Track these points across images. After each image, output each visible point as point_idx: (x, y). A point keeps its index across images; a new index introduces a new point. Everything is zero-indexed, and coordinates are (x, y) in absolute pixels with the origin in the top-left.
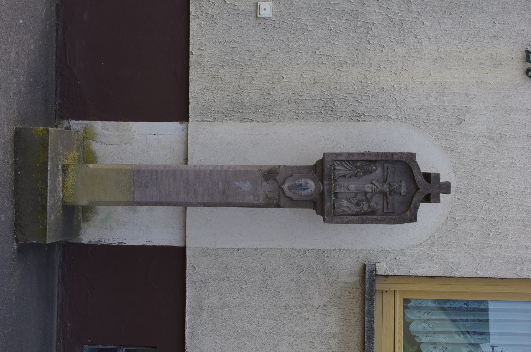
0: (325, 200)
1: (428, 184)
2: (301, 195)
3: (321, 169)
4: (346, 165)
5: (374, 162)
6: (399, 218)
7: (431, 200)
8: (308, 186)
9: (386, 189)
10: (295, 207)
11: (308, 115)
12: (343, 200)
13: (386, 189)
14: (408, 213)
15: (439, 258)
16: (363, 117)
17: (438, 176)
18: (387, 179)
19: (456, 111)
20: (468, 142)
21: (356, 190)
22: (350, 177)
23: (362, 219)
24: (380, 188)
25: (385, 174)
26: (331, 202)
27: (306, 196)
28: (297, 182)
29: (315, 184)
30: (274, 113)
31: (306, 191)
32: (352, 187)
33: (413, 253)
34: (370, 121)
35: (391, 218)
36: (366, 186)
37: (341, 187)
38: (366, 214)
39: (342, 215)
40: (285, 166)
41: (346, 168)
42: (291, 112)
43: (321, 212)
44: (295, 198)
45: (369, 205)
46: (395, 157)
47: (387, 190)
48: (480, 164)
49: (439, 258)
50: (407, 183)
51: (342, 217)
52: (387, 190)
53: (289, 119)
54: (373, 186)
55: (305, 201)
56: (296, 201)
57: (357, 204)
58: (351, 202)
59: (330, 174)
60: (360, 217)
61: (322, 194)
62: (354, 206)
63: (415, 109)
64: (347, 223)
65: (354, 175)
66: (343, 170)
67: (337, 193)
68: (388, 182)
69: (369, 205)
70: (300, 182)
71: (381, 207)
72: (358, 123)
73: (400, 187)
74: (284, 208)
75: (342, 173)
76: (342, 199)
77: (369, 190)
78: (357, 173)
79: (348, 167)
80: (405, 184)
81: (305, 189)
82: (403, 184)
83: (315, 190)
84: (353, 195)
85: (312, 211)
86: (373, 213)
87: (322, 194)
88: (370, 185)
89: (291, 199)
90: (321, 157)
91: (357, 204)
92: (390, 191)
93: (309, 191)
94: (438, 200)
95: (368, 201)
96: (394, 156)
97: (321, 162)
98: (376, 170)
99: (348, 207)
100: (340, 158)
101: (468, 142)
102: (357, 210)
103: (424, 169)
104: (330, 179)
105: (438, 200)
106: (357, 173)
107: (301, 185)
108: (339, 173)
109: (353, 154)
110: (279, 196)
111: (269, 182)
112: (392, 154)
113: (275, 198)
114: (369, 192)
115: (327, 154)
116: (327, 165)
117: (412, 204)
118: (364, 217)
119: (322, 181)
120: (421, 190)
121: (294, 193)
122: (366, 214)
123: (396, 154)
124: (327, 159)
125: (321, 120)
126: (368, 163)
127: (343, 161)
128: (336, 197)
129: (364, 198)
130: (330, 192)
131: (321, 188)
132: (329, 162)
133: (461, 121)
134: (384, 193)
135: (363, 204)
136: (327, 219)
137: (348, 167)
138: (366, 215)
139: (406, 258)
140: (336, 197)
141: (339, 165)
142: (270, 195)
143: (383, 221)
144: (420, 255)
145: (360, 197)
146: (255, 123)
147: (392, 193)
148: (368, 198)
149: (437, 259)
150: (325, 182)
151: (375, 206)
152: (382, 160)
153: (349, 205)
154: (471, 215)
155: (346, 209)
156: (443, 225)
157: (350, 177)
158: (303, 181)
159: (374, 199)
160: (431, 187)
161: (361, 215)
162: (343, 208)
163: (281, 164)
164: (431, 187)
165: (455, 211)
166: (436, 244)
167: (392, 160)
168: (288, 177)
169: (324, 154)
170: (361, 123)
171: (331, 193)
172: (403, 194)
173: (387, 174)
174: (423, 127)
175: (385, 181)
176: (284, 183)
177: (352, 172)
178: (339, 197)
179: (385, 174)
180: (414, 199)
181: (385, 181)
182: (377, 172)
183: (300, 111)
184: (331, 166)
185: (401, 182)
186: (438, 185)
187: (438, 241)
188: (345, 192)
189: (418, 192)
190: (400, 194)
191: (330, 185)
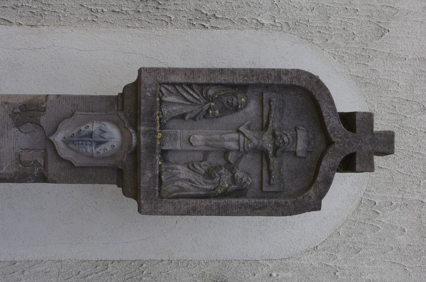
0: (142, 166)
1: (350, 134)
2: (92, 156)
3: (135, 102)
4: (185, 94)
5: (243, 88)
6: (294, 203)
7: (358, 167)
8: (106, 136)
9: (267, 143)
10: (79, 182)
11: (115, 15)
12: (179, 167)
13: (267, 143)
14: (311, 192)
15: (347, 272)
16: (213, 20)
17: (369, 117)
18: (268, 123)
19: (375, 14)
20: (395, 69)
21: (206, 145)
22: (194, 119)
23: (217, 204)
24: (255, 141)
25: (265, 113)
26: (153, 169)
27: (103, 158)
28: (83, 128)
29: (122, 133)
30: (50, 9)
31: (102, 147)
32: (199, 139)
33: (302, 264)
34: (226, 28)
35: (276, 203)
36: (226, 137)
37: (176, 139)
38: (226, 194)
39: (177, 197)
40: (58, 96)
41: (189, 101)
42: (83, 10)
43: (133, 191)
44: (78, 161)
45: (233, 177)
46: (284, 78)
47: (269, 146)
48: (415, 107)
49: (347, 272)
50: (308, 131)
51: (176, 201)
52: (269, 146)
53: (79, 21)
54: (242, 137)
55: (101, 168)
56: (82, 168)
57: (209, 175)
58: (195, 171)
59: (152, 113)
60: (214, 201)
61: (135, 153)
62: (201, 179)
63: (304, 9)
64: (188, 213)
65: (203, 113)
66: (179, 104)
67: (166, 151)
68: (270, 130)
69: (233, 177)
70: (90, 129)
71: (256, 180)
72: (204, 31)
73: (295, 139)
74: (55, 182)
75: (176, 109)
76: (177, 163)
77: (233, 145)
78: (207, 111)
79: (189, 97)
80: (304, 133)
81: (99, 143)
82: (301, 134)
83: (121, 146)
84: (199, 156)
85: (113, 190)
86: (240, 192)
87: (135, 153)
88: (235, 136)
89: (70, 163)
90: (133, 78)
91: (209, 175)
92: (276, 148)
93: (108, 147)
94: (369, 167)
95: (231, 168)
96: (283, 77)
97: (134, 89)
98: (246, 105)
99: (190, 181)
100: (173, 79)
101: (395, 69)
102: (209, 187)
103: (343, 105)
104: (153, 122)
105: (369, 167)
106: (207, 111)
107: (91, 135)
108: (170, 109)
109: (199, 70)
110: (45, 158)
111: (23, 128)
112: (279, 73)
113: (36, 161)
114: (232, 151)
115: (146, 69)
116: (147, 92)
117: (320, 175)
118: (222, 201)
119: (135, 126)
120: (336, 146)
121: (77, 152)
122: (226, 194)
123: (287, 72)
124: (147, 80)
125: (137, 25)
126: (231, 91)
127: (181, 84)
128: (165, 160)
129: (222, 162)
130: (152, 148)
131: (134, 141)
132: (150, 86)
133: (382, 32)
134: (263, 153)
135: (220, 175)
136: (145, 207)
137: (189, 97)
138: (227, 196)
139: (290, 274)
140: (165, 160)
141: (171, 93)
142: (26, 157)
143: (260, 208)
144: (314, 269)
145: (214, 159)
146: (15, 28)
147: (278, 152)
148: (229, 163)
149: (343, 274)
150: (142, 128)
151: (244, 179)
152: (258, 85)
153: (190, 175)
154: (400, 196)
155: (186, 185)
156: (353, 213)
157: (194, 119)
158: (94, 127)
159: (242, 164)
160: (355, 143)
161: (215, 197)
162: (180, 183)
163: (52, 91)
164: (355, 143)
165: (373, 189)
166: (341, 248)
167: (279, 86)
168: (63, 119)
169: (140, 71)
170: (210, 31)
171: (154, 152)
172: (299, 154)
173: (269, 113)
174: (317, 41)
175: (264, 128)
176: (55, 131)
177: (197, 109)
178: (171, 160)
179: (265, 113)
180: (323, 163)
181: (264, 128)
182: (248, 109)
183: (99, 8)
184: (154, 95)
185: (296, 129)
186: (369, 136)
187: (344, 242)
188: (183, 151)
189: (331, 149)
190: (295, 153)
191: (152, 134)
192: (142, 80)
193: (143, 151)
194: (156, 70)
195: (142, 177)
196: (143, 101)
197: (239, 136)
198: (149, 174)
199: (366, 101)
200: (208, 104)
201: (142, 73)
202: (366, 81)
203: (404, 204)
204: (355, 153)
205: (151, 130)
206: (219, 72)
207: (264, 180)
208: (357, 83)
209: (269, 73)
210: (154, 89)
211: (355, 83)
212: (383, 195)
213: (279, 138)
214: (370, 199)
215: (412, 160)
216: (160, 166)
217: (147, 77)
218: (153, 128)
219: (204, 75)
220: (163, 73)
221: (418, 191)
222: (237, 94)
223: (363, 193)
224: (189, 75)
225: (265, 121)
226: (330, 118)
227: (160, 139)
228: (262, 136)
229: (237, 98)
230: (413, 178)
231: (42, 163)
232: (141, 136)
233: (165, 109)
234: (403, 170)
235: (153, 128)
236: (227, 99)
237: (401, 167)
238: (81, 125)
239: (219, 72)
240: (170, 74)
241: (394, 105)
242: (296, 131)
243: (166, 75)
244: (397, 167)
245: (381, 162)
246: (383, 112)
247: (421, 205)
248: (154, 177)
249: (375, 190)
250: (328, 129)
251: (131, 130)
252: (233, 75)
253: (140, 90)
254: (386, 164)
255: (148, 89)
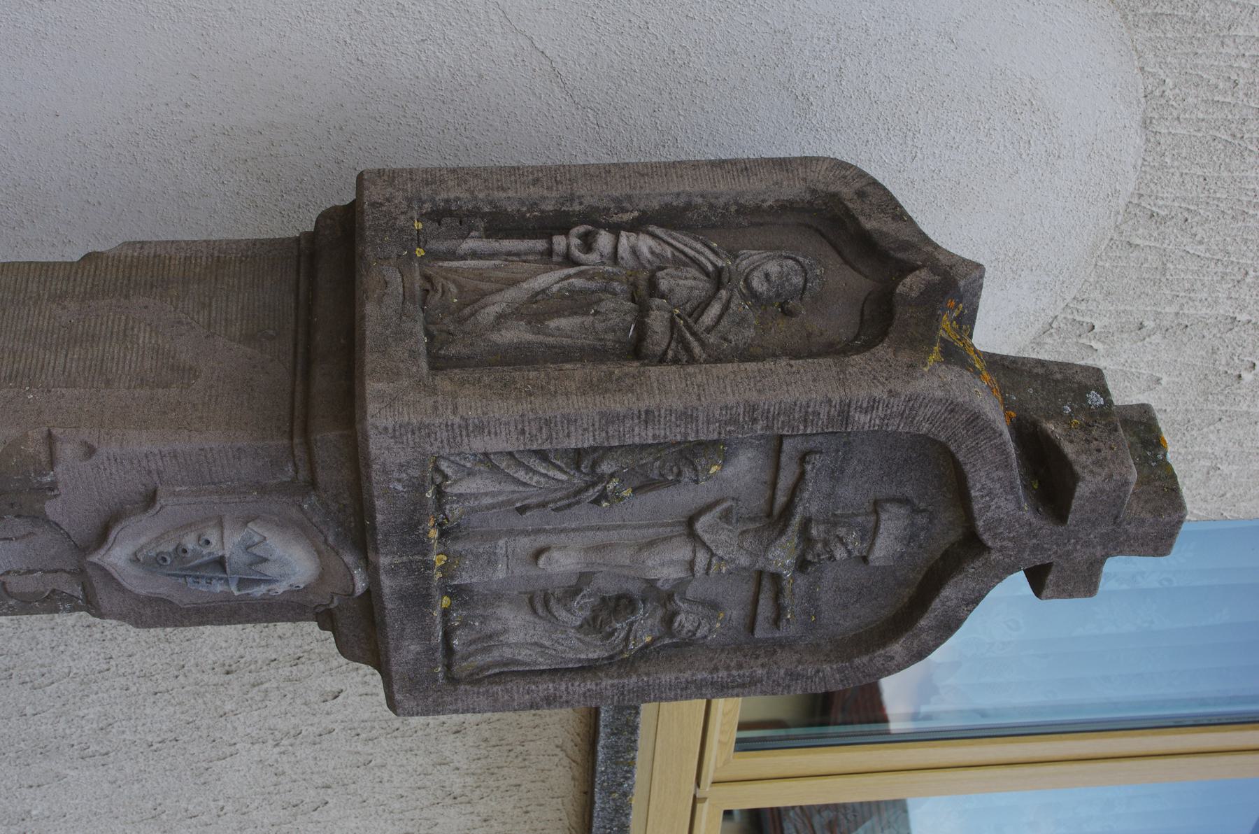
28: (190, 542)
68: (796, 521)
70: (215, 549)
120: (995, 556)
169: (360, 178)
176: (102, 536)
192: (373, 457)
193: (390, 606)
194: (420, 429)
195: (392, 653)
196: (379, 503)
197: (694, 552)
198: (412, 647)
199: (1142, 69)
200: (599, 487)
201: (371, 441)
202: (1158, 10)
203: (1179, 324)
204: (1050, 565)
205: (411, 562)
206: (639, 417)
207: (760, 618)
208: (1124, 17)
209: (810, 410)
210: (415, 473)
211: (1118, 16)
212: (1122, 308)
213: (820, 546)
214: (1078, 318)
215: (1240, 224)
216: (446, 613)
217: (388, 449)
218: (417, 558)
219: (585, 430)
220: (445, 434)
221: (1233, 295)
222: (695, 456)
223: (1063, 305)
224: (534, 432)
225: (781, 499)
226: (992, 500)
227: (442, 568)
228: (766, 549)
229: (695, 469)
230: (1227, 266)
231: (78, 592)
232: (383, 577)
233: (455, 506)
234: (1202, 248)
235: (417, 558)
236: (662, 467)
237: (1201, 243)
238: (187, 526)
239: (639, 417)
240: (468, 435)
241: (1234, 77)
242: (876, 512)
243: (454, 438)
244: (1186, 240)
245: (1141, 231)
246: (1190, 100)
247: (1230, 326)
248: (431, 650)
249: (1100, 297)
250: (980, 523)
251: (349, 558)
252: (686, 424)
253: (369, 478)
254: (1155, 234)
255: (396, 475)
